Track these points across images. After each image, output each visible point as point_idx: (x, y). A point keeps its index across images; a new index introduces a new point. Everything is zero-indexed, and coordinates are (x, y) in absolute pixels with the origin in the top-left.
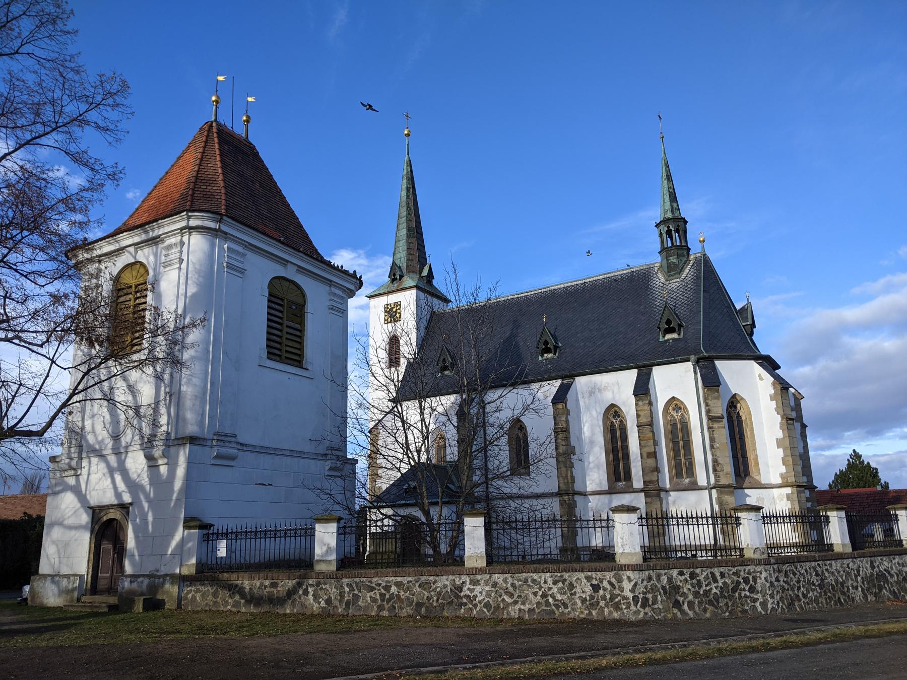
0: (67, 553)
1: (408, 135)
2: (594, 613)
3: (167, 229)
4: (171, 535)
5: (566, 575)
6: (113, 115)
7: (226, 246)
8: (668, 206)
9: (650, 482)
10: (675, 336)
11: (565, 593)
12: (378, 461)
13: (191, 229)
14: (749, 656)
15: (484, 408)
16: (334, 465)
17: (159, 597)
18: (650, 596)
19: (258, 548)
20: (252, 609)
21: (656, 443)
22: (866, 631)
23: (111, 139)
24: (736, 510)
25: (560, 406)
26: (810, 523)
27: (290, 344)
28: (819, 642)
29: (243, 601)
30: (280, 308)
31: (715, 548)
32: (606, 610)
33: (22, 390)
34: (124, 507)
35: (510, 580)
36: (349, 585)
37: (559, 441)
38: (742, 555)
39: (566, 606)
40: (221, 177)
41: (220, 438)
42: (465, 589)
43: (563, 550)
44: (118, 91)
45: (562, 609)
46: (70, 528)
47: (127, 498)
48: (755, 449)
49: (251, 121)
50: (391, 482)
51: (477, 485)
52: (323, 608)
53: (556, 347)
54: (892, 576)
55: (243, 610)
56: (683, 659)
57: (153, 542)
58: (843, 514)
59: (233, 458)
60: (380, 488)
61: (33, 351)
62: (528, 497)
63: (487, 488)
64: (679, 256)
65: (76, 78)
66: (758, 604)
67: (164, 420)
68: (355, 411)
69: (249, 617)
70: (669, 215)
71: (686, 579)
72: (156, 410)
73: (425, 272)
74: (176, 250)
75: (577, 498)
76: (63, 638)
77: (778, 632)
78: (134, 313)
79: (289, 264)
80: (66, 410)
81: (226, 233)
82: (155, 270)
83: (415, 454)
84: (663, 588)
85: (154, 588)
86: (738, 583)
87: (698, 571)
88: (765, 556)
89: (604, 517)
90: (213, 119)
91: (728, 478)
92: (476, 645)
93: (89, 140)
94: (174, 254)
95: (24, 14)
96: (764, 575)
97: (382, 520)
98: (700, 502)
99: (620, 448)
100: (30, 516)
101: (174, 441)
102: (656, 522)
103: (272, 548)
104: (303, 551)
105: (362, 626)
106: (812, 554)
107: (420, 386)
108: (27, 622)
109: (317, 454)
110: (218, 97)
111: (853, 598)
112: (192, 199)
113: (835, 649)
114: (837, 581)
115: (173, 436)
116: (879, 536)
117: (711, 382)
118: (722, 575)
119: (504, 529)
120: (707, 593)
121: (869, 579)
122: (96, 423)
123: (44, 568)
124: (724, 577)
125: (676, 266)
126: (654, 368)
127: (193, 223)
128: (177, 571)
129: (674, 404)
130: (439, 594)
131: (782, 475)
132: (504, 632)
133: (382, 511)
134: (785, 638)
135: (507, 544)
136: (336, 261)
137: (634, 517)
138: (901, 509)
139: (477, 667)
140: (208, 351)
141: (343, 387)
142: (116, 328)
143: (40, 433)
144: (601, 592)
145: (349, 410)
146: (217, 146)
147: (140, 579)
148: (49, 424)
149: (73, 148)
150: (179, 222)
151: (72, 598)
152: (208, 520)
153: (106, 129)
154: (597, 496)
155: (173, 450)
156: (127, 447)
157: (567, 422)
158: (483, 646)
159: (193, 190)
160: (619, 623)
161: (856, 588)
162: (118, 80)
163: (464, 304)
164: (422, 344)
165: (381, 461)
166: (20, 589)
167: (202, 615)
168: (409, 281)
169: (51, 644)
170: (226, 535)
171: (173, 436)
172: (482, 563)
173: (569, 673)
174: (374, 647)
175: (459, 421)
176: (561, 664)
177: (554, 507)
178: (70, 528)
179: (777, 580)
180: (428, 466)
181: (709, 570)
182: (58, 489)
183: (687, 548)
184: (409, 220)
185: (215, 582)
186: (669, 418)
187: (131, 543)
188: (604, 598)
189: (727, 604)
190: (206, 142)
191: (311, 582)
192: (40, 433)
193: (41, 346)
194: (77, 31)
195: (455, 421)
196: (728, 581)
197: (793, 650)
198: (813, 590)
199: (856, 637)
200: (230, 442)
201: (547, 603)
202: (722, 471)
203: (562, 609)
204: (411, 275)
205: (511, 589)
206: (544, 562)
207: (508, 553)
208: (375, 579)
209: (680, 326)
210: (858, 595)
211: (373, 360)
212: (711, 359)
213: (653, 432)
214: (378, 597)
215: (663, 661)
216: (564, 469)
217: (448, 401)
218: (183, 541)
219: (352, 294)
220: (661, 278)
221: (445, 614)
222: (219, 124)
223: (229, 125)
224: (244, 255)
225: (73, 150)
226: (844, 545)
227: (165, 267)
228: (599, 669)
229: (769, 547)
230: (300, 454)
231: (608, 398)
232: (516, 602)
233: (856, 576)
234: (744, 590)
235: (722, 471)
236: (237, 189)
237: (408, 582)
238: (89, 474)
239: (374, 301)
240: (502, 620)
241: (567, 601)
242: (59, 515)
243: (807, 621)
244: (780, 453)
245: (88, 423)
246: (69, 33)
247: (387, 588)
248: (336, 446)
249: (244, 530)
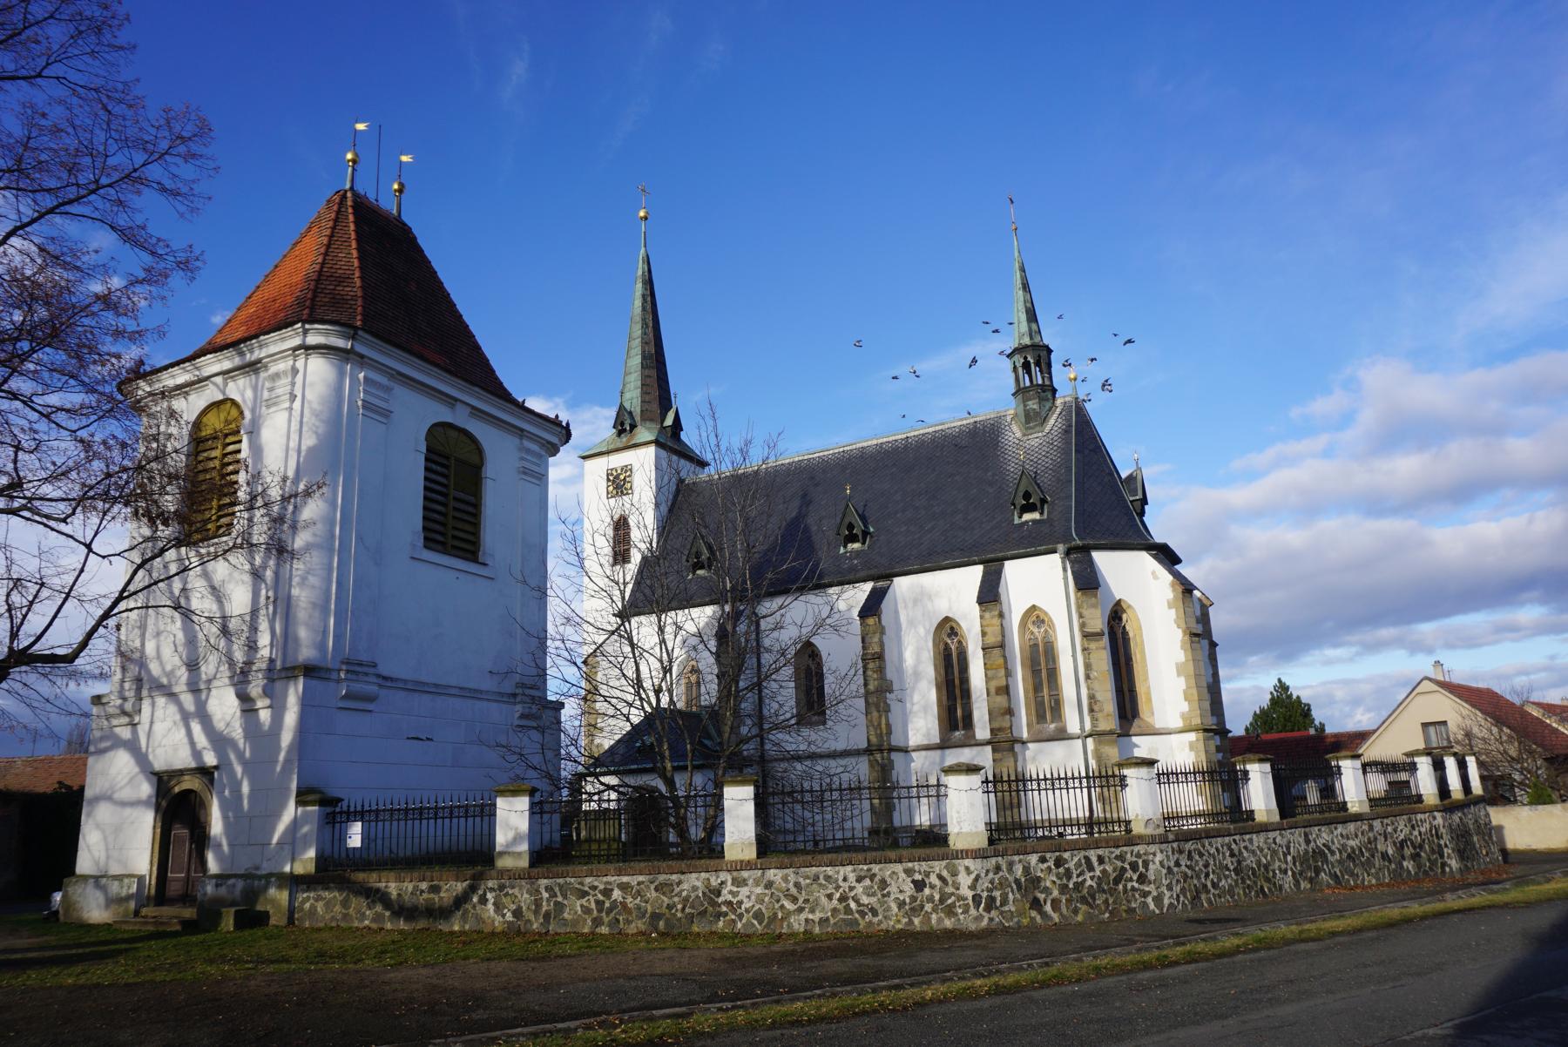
0: (119, 841)
2: (916, 921)
3: (273, 349)
4: (277, 815)
5: (876, 868)
6: (187, 171)
7: (361, 376)
8: (1024, 327)
9: (1000, 729)
10: (1036, 516)
11: (874, 895)
12: (598, 705)
13: (308, 349)
14: (1140, 976)
15: (758, 625)
17: (259, 908)
18: (997, 894)
19: (409, 834)
20: (402, 925)
21: (1009, 673)
22: (1301, 932)
23: (182, 209)
24: (1120, 765)
25: (871, 621)
26: (1223, 781)
27: (460, 525)
28: (1236, 951)
29: (387, 914)
31: (1091, 823)
32: (934, 916)
33: (45, 593)
34: (205, 772)
35: (792, 878)
36: (547, 889)
37: (869, 673)
38: (1129, 831)
39: (874, 912)
40: (357, 274)
42: (725, 892)
43: (874, 832)
45: (869, 917)
46: (124, 804)
47: (210, 759)
48: (1146, 679)
50: (617, 737)
51: (747, 740)
52: (509, 923)
53: (866, 533)
54: (1333, 853)
55: (389, 926)
56: (1044, 985)
57: (250, 826)
58: (1267, 767)
59: (371, 699)
62: (821, 756)
63: (762, 744)
64: (1042, 400)
65: (130, 113)
66: (1149, 900)
67: (264, 639)
68: (561, 629)
69: (397, 937)
70: (1027, 341)
71: (1049, 868)
72: (254, 629)
73: (669, 421)
74: (285, 381)
75: (895, 756)
76: (101, 973)
77: (1178, 939)
79: (459, 405)
80: (111, 622)
81: (362, 356)
82: (253, 411)
83: (652, 694)
84: (1017, 881)
85: (252, 895)
86: (1123, 870)
87: (1066, 855)
88: (1161, 831)
89: (933, 781)
90: (348, 186)
91: (1109, 723)
92: (739, 974)
93: (150, 209)
94: (283, 387)
95: (52, 17)
96: (1159, 857)
97: (599, 793)
98: (1069, 757)
99: (957, 682)
100: (69, 788)
101: (280, 673)
102: (1008, 788)
103: (434, 834)
104: (478, 839)
105: (568, 949)
106: (1226, 825)
107: (659, 592)
108: (54, 948)
110: (356, 155)
111: (1281, 887)
112: (314, 303)
113: (1260, 960)
114: (1259, 863)
115: (279, 665)
116: (1313, 797)
117: (1087, 581)
118: (1101, 860)
119: (784, 804)
120: (1078, 886)
121: (1303, 859)
122: (163, 648)
123: (84, 864)
124: (1102, 862)
125: (1037, 414)
126: (1007, 563)
127: (312, 339)
128: (287, 869)
129: (1034, 616)
130: (686, 900)
131: (1183, 716)
132: (783, 954)
133: (602, 779)
134: (1188, 947)
135: (789, 826)
136: (536, 404)
137: (976, 780)
138: (1346, 757)
139: (742, 1007)
140: (333, 536)
142: (197, 498)
143: (70, 658)
144: (927, 891)
146: (352, 227)
147: (231, 881)
148: (84, 645)
149: (122, 220)
150: (290, 339)
151: (126, 910)
152: (337, 793)
153: (175, 193)
154: (924, 753)
155: (279, 685)
156: (209, 681)
157: (882, 644)
158: (749, 975)
160: (951, 935)
161: (1285, 872)
162: (193, 117)
163: (726, 469)
164: (666, 525)
165: (600, 706)
166: (47, 899)
167: (325, 935)
168: (645, 433)
169: (82, 980)
170: (360, 815)
171: (279, 665)
172: (751, 853)
173: (875, 1011)
174: (584, 980)
175: (719, 645)
176: (864, 999)
177: (862, 769)
178: (124, 804)
179: (1177, 864)
180: (673, 712)
181: (1083, 853)
182: (103, 745)
183: (1051, 824)
184: (645, 343)
185: (344, 884)
186: (1028, 636)
187: (216, 826)
188: (930, 899)
189: (1106, 901)
190: (336, 220)
192: (70, 658)
195: (713, 644)
196: (1109, 868)
197: (1200, 965)
198: (1226, 877)
199: (1288, 942)
201: (848, 910)
202: (1101, 711)
203: (869, 917)
204: (648, 424)
205: (794, 891)
206: (846, 850)
207: (791, 838)
208: (588, 880)
209: (1043, 501)
210: (1288, 881)
211: (588, 551)
212: (1086, 550)
213: (1005, 657)
214: (593, 906)
215: (1016, 989)
216: (875, 714)
217: (701, 617)
218: (295, 824)
219: (554, 451)
220: (1016, 431)
221: (695, 929)
222: (356, 195)
223: (372, 197)
224: (388, 390)
225: (122, 223)
226: (1268, 811)
227: (268, 407)
228: (921, 1004)
229: (1167, 818)
230: (474, 694)
231: (942, 608)
232: (801, 910)
233: (1285, 855)
234: (1131, 880)
235: (1101, 711)
236: (386, 296)
237: (639, 884)
238: (152, 723)
239: (589, 463)
240: (780, 936)
241: (876, 906)
242: (107, 785)
243: (1218, 921)
244: (1181, 683)
245: (150, 648)
246: (122, 48)
247: (607, 892)
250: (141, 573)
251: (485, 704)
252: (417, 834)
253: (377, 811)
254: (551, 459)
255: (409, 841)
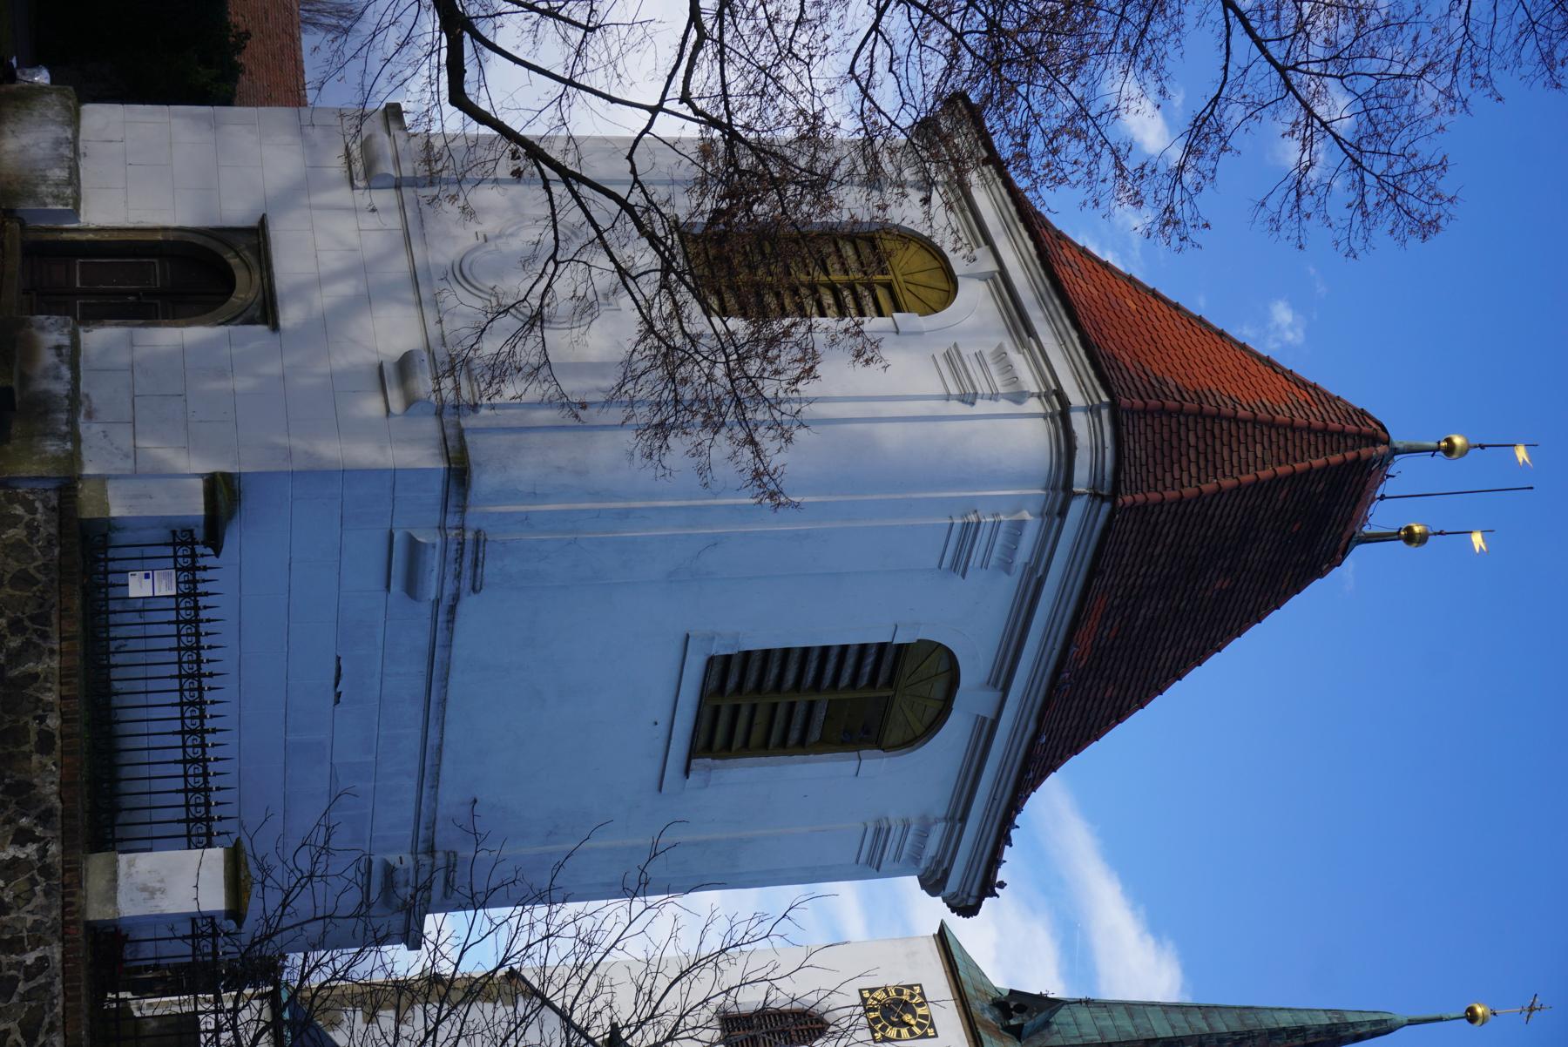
0: (138, 168)
1: (1471, 1016)
7: (1026, 515)
12: (418, 1010)
13: (1061, 415)
16: (400, 877)
19: (153, 685)
23: (1273, 204)
27: (760, 718)
30: (864, 681)
33: (576, 35)
34: (266, 312)
36: (42, 962)
41: (469, 548)
44: (1408, 213)
47: (290, 315)
49: (1412, 549)
59: (412, 587)
60: (335, 1024)
61: (670, 78)
68: (570, 931)
78: (813, 288)
79: (995, 696)
81: (1063, 513)
100: (239, 48)
103: (150, 720)
109: (432, 825)
110: (1464, 452)
123: (100, 119)
127: (1080, 423)
141: (635, 885)
145: (572, 908)
146: (1318, 462)
147: (66, 373)
149: (1234, 113)
159: (1180, 411)
166: (35, 64)
170: (190, 594)
187: (168, 338)
190: (1325, 431)
191: (54, 848)
193: (685, 98)
194: (1558, 86)
200: (458, 576)
219: (933, 885)
222: (1385, 461)
223: (1387, 487)
224: (1006, 566)
230: (429, 773)
236: (1209, 512)
248: (460, 878)
249: (204, 641)
250: (614, 207)
251: (412, 796)
252: (154, 699)
253: (197, 622)
254: (913, 882)
255: (140, 686)
